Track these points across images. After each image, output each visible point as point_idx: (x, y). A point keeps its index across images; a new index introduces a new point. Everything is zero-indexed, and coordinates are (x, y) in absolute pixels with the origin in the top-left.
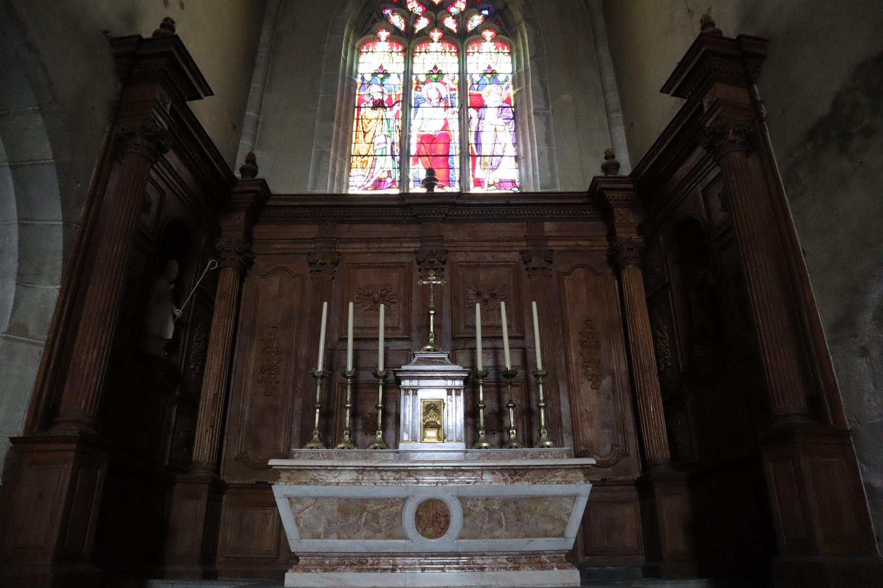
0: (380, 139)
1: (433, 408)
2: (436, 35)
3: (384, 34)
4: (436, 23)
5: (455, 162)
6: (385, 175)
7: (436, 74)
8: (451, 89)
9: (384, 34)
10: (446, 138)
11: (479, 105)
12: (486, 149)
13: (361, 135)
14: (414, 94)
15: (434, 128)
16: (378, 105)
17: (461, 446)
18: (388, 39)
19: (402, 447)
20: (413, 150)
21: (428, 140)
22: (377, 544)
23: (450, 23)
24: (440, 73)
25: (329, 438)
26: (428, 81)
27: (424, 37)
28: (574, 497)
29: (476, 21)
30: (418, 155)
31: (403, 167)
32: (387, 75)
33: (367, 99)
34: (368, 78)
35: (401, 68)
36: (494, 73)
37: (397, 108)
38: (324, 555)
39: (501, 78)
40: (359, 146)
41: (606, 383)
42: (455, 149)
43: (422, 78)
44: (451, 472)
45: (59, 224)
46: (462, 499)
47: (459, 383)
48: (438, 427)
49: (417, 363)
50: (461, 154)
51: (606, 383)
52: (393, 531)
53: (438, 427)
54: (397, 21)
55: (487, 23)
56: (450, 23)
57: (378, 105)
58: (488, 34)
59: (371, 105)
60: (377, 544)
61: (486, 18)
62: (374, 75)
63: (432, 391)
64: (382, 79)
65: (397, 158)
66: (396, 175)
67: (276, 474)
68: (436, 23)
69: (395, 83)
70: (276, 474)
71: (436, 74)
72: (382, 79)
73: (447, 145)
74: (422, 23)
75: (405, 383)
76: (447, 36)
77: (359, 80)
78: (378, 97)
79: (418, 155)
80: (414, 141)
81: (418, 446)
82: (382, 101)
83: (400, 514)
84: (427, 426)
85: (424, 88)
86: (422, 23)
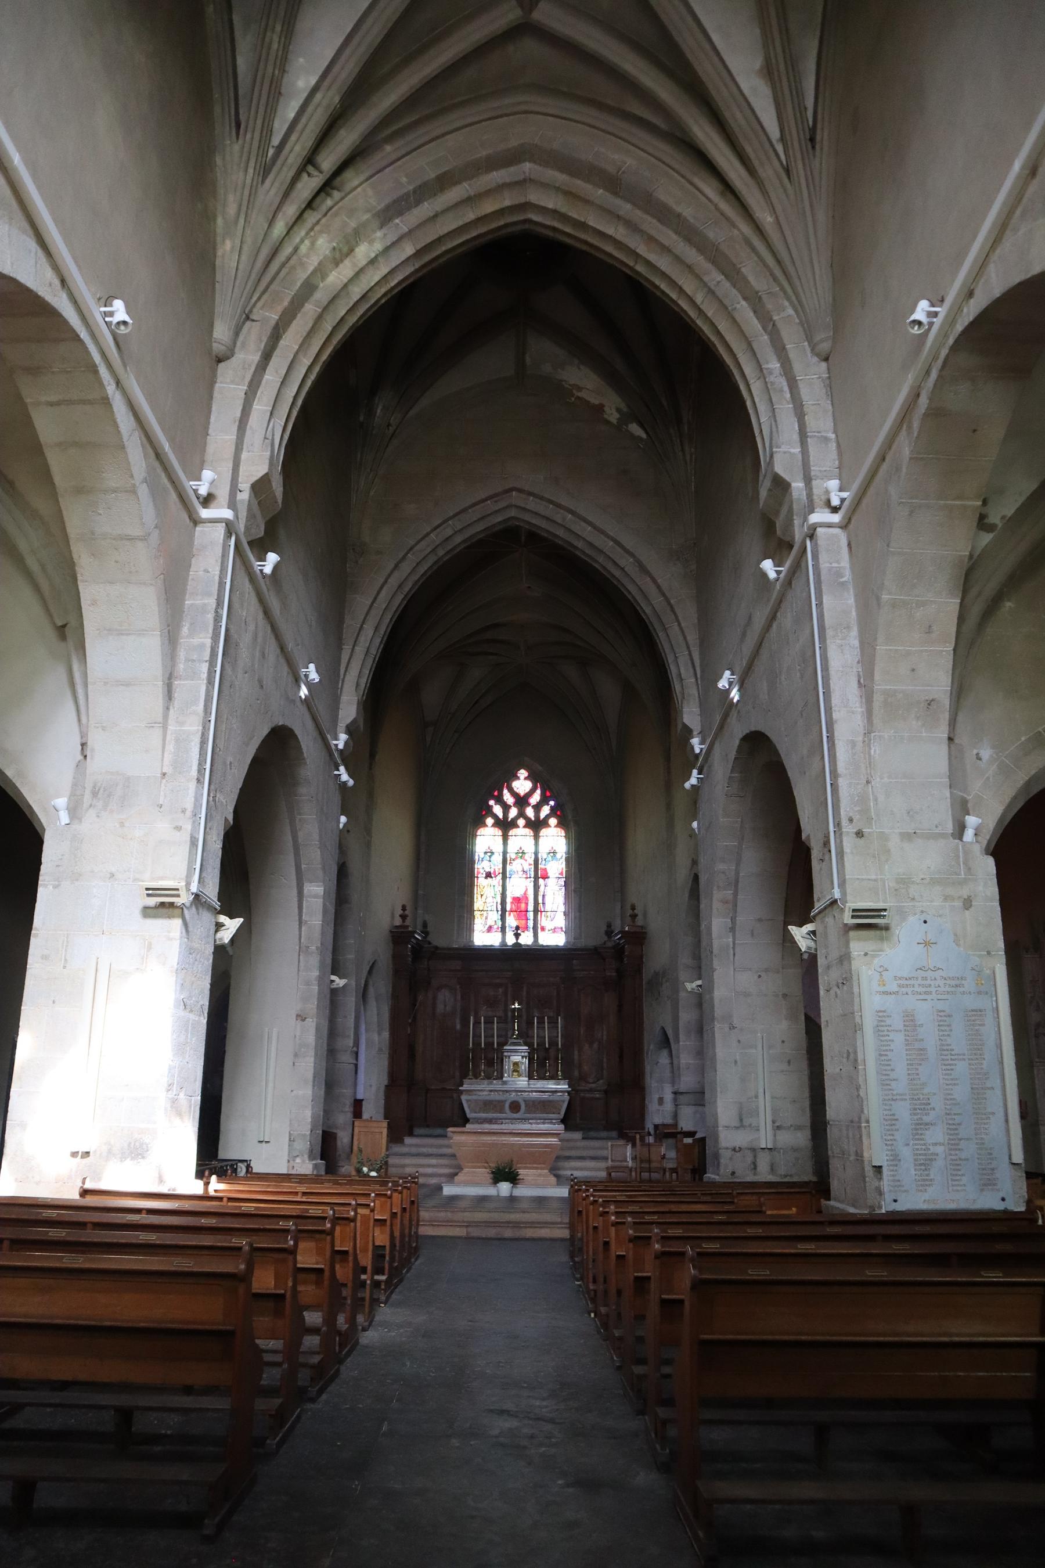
0: (489, 900)
1: (516, 1064)
2: (521, 822)
3: (490, 821)
4: (521, 814)
5: (531, 915)
6: (493, 924)
7: (521, 854)
8: (530, 865)
9: (490, 821)
10: (525, 896)
11: (545, 877)
12: (548, 907)
13: (479, 896)
14: (508, 868)
15: (519, 893)
16: (488, 875)
17: (527, 1079)
18: (494, 825)
19: (504, 1079)
20: (508, 908)
21: (517, 900)
22: (495, 1115)
23: (530, 812)
24: (523, 853)
25: (476, 1076)
26: (516, 858)
27: (513, 824)
28: (564, 1101)
29: (545, 810)
30: (511, 911)
31: (503, 918)
32: (492, 853)
33: (482, 871)
34: (482, 855)
35: (501, 848)
36: (554, 853)
37: (500, 877)
38: (480, 1119)
39: (558, 856)
40: (478, 904)
41: (595, 1045)
42: (531, 907)
43: (513, 856)
44: (830, 909)
45: (616, 1233)
46: (525, 1101)
47: (526, 1054)
48: (518, 1071)
49: (510, 1045)
50: (534, 911)
51: (595, 1045)
52: (502, 1111)
53: (518, 1071)
54: (498, 810)
55: (553, 812)
56: (530, 812)
57: (488, 875)
58: (553, 821)
59: (484, 875)
60: (495, 1115)
61: (552, 808)
62: (486, 853)
63: (516, 1058)
64: (490, 857)
65: (500, 913)
66: (500, 923)
67: (462, 1092)
68: (521, 814)
69: (498, 859)
70: (462, 1092)
71: (521, 854)
72: (490, 857)
73: (527, 904)
74: (513, 812)
75: (505, 1054)
76: (529, 824)
77: (477, 858)
78: (488, 870)
79: (511, 911)
80: (509, 900)
81: (509, 1079)
82: (490, 873)
83: (504, 1105)
84: (514, 1071)
85: (514, 863)
86: (513, 812)
